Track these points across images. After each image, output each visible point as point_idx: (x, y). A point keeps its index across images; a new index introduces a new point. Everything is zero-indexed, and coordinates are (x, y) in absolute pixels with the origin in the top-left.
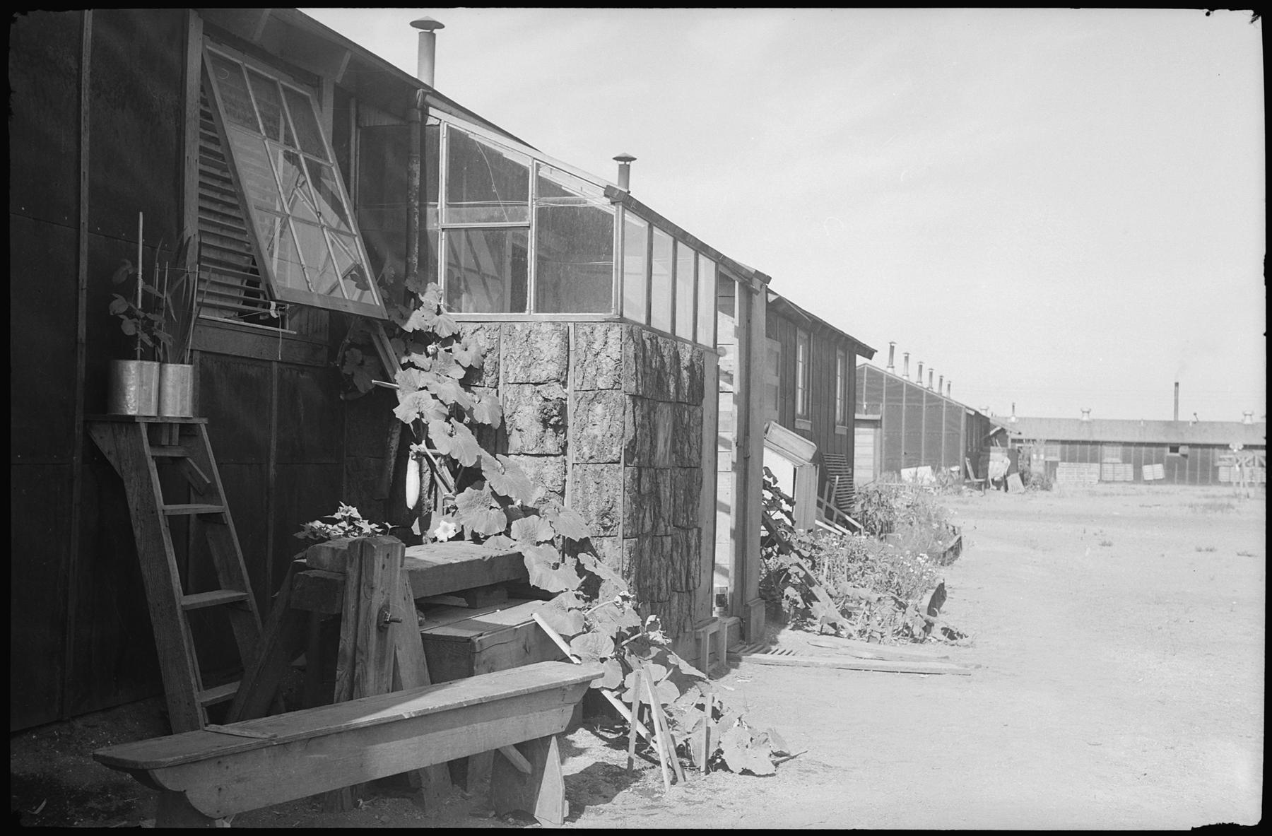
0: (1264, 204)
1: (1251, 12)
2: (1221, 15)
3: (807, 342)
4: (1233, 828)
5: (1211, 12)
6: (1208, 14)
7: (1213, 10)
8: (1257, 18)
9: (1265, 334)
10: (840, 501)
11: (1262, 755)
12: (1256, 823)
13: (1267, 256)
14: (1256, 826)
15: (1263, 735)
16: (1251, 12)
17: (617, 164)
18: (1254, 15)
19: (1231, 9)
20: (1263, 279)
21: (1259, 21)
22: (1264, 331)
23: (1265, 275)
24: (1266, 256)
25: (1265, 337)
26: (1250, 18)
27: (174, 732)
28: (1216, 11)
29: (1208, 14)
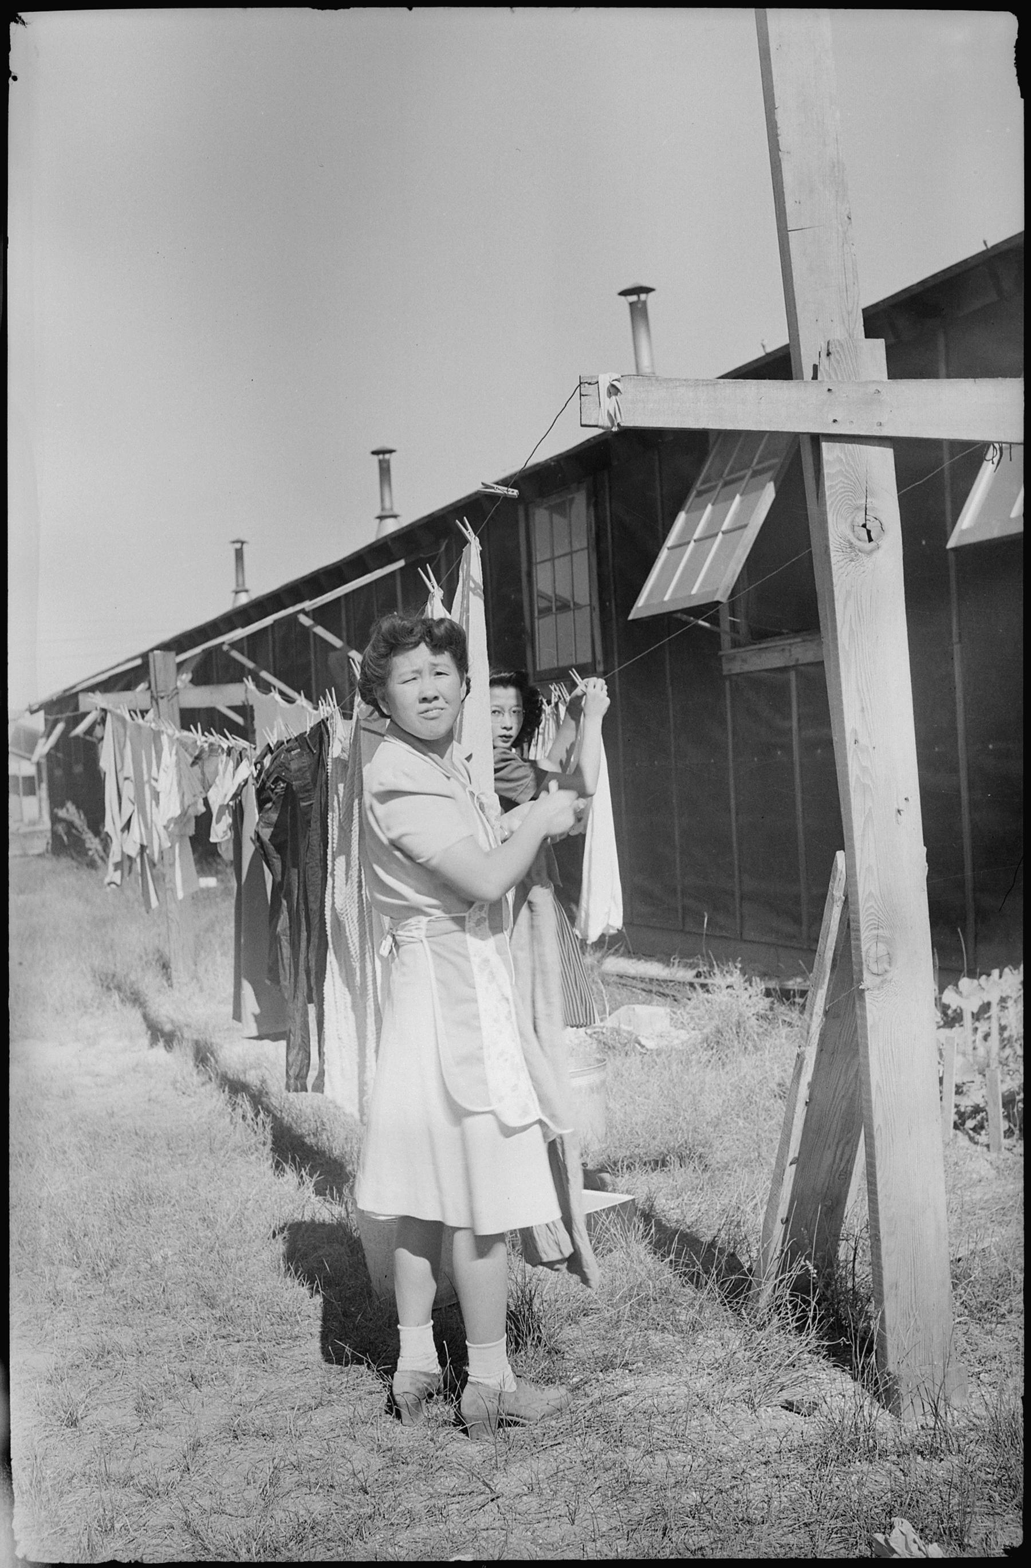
0: (249, 10)
1: (13, 26)
2: (16, 62)
3: (49, 726)
4: (1020, 47)
5: (13, 75)
6: (15, 78)
7: (10, 72)
8: (20, 18)
9: (410, 9)
10: (266, 730)
11: (11, 1179)
12: (1015, 18)
13: (344, 8)
14: (1018, 19)
15: (1022, 659)
16: (13, 26)
17: (375, 459)
18: (17, 22)
19: (9, 50)
20: (341, 11)
21: (23, 15)
22: (405, 9)
23: (336, 9)
24: (313, 8)
25: (414, 8)
26: (20, 26)
27: (794, 376)
28: (11, 69)
29: (15, 78)
